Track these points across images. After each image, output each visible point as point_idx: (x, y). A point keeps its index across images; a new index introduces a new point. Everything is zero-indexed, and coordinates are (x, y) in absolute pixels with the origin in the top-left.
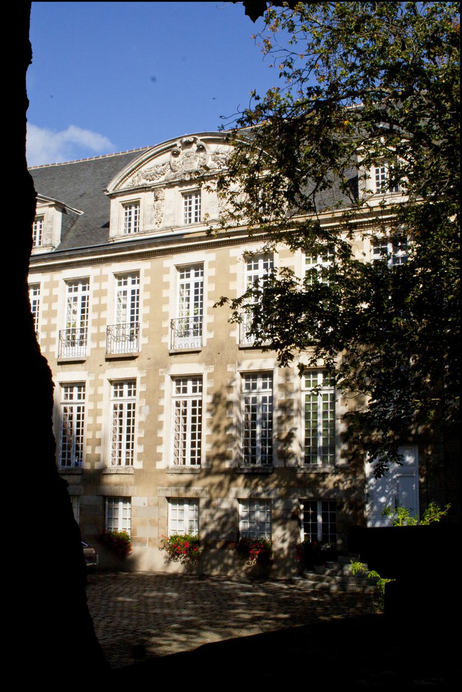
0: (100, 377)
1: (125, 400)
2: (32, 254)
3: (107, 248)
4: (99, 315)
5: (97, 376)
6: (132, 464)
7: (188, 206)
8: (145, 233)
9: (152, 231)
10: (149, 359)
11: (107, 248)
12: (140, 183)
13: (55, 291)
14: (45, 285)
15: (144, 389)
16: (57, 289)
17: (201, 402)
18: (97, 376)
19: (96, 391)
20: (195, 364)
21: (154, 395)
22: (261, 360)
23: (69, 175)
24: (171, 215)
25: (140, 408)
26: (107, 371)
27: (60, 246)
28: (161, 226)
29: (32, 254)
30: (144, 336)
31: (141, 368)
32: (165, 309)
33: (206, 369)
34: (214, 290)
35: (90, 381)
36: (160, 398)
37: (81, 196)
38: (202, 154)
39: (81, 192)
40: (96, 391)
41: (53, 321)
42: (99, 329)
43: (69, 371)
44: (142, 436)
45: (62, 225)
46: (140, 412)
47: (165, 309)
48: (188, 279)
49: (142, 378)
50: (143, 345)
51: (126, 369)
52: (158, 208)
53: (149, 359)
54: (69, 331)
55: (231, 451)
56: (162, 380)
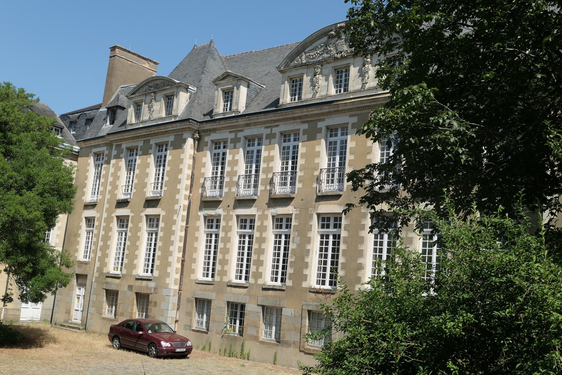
3: (163, 129)
6: (285, 282)
7: (294, 88)
8: (306, 101)
10: (302, 200)
11: (163, 129)
14: (231, 141)
15: (297, 224)
17: (339, 236)
20: (336, 205)
21: (305, 229)
23: (260, 60)
25: (294, 238)
27: (244, 111)
30: (300, 182)
32: (316, 161)
34: (354, 146)
35: (259, 215)
37: (266, 75)
39: (267, 71)
44: (293, 260)
45: (247, 95)
46: (293, 242)
47: (316, 161)
48: (289, 143)
49: (296, 215)
50: (298, 188)
53: (302, 200)
56: (311, 216)
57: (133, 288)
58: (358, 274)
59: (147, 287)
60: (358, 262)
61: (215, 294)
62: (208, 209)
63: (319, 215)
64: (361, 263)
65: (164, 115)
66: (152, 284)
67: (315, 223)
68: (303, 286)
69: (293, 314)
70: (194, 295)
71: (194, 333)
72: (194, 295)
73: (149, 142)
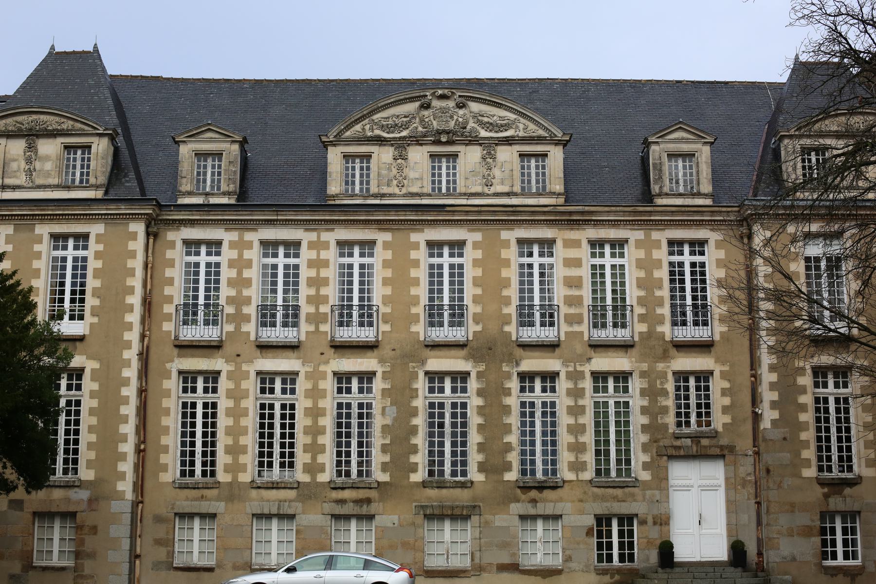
53: (394, 350)
56: (415, 376)
57: (26, 505)
58: (506, 457)
59: (68, 500)
60: (504, 441)
61: (223, 504)
62: (703, 355)
63: (427, 373)
64: (510, 443)
65: (428, 189)
66: (84, 495)
67: (421, 384)
68: (411, 480)
69: (396, 522)
70: (173, 508)
71: (180, 573)
72: (173, 508)
73: (34, 230)
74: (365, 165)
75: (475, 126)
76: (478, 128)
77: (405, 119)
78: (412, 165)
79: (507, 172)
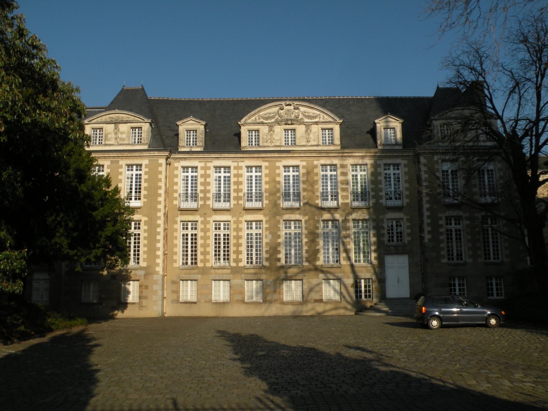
0: (240, 219)
1: (254, 231)
2: (526, 160)
4: (238, 187)
5: (238, 219)
9: (268, 146)
12: (260, 121)
13: (208, 172)
15: (268, 226)
16: (209, 171)
18: (238, 219)
19: (238, 226)
22: (351, 216)
24: (278, 140)
26: (244, 216)
28: (273, 144)
29: (526, 160)
31: (265, 215)
33: (303, 218)
35: (234, 221)
36: (278, 231)
38: (296, 111)
40: (238, 226)
41: (240, 187)
42: (238, 194)
43: (220, 215)
50: (265, 204)
51: (256, 216)
52: (271, 135)
54: (248, 193)
55: (344, 260)
56: (279, 222)
74: (287, 133)
75: (303, 117)
76: (304, 118)
77: (273, 115)
78: (276, 134)
79: (316, 136)
